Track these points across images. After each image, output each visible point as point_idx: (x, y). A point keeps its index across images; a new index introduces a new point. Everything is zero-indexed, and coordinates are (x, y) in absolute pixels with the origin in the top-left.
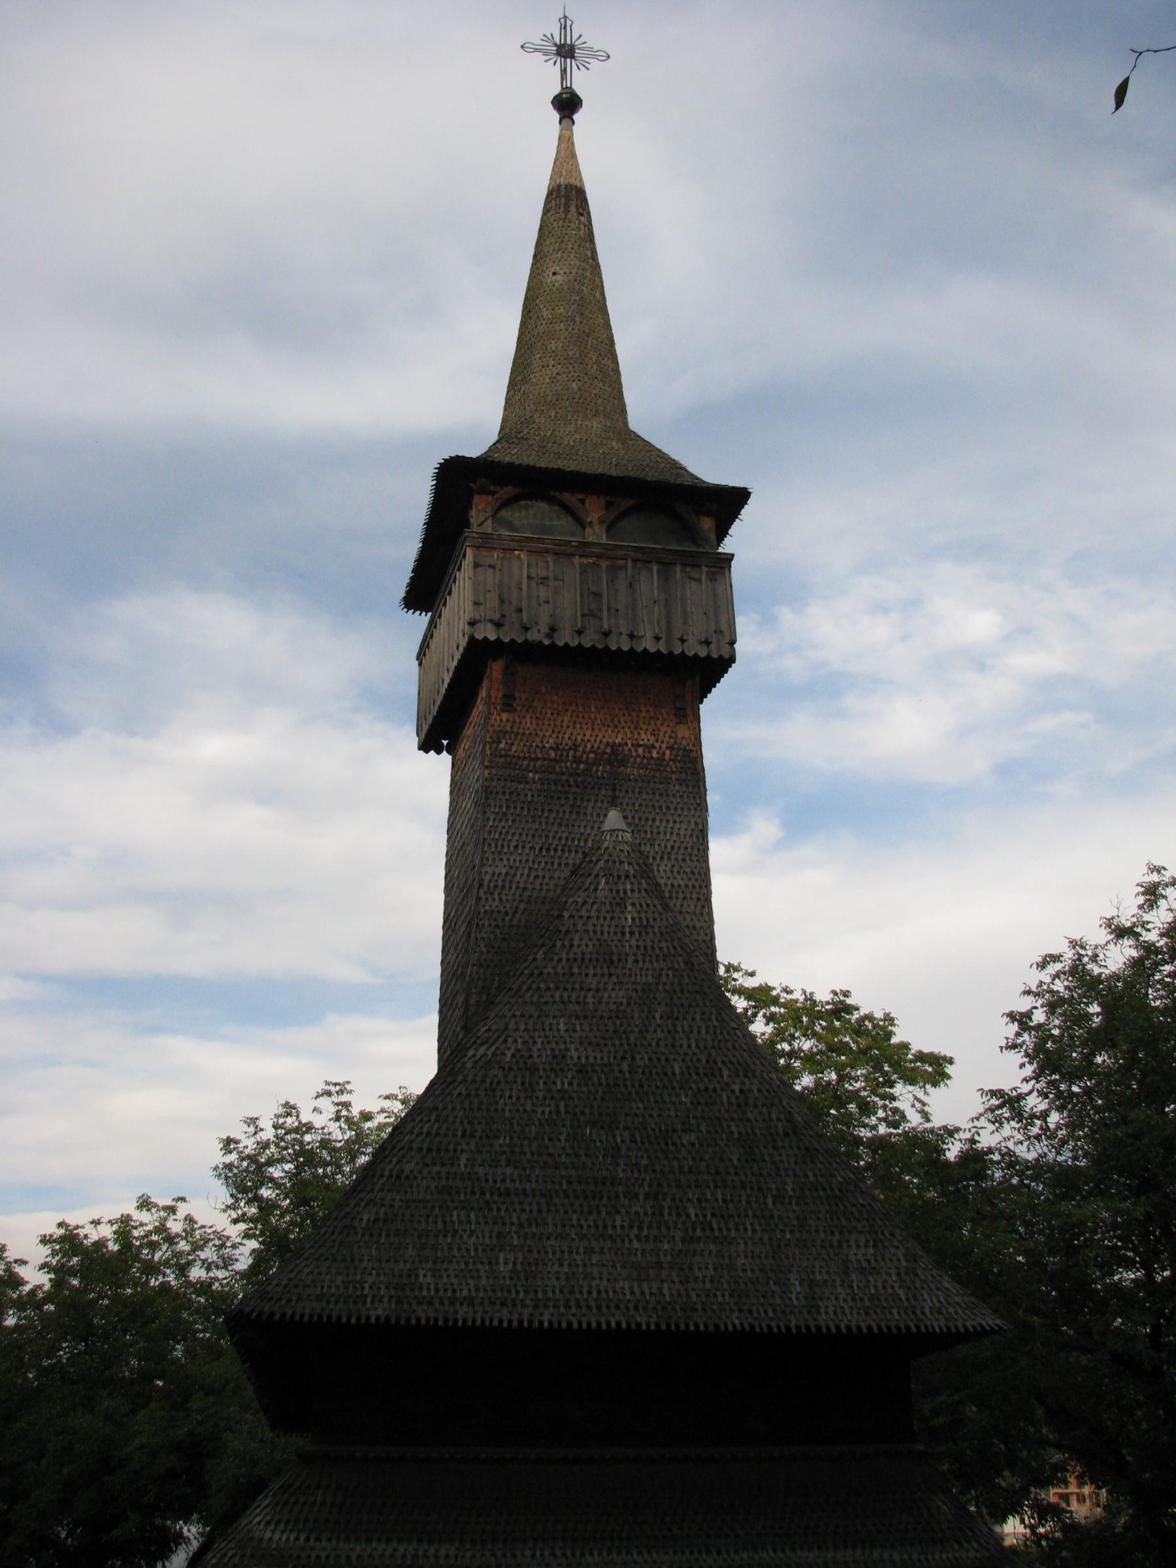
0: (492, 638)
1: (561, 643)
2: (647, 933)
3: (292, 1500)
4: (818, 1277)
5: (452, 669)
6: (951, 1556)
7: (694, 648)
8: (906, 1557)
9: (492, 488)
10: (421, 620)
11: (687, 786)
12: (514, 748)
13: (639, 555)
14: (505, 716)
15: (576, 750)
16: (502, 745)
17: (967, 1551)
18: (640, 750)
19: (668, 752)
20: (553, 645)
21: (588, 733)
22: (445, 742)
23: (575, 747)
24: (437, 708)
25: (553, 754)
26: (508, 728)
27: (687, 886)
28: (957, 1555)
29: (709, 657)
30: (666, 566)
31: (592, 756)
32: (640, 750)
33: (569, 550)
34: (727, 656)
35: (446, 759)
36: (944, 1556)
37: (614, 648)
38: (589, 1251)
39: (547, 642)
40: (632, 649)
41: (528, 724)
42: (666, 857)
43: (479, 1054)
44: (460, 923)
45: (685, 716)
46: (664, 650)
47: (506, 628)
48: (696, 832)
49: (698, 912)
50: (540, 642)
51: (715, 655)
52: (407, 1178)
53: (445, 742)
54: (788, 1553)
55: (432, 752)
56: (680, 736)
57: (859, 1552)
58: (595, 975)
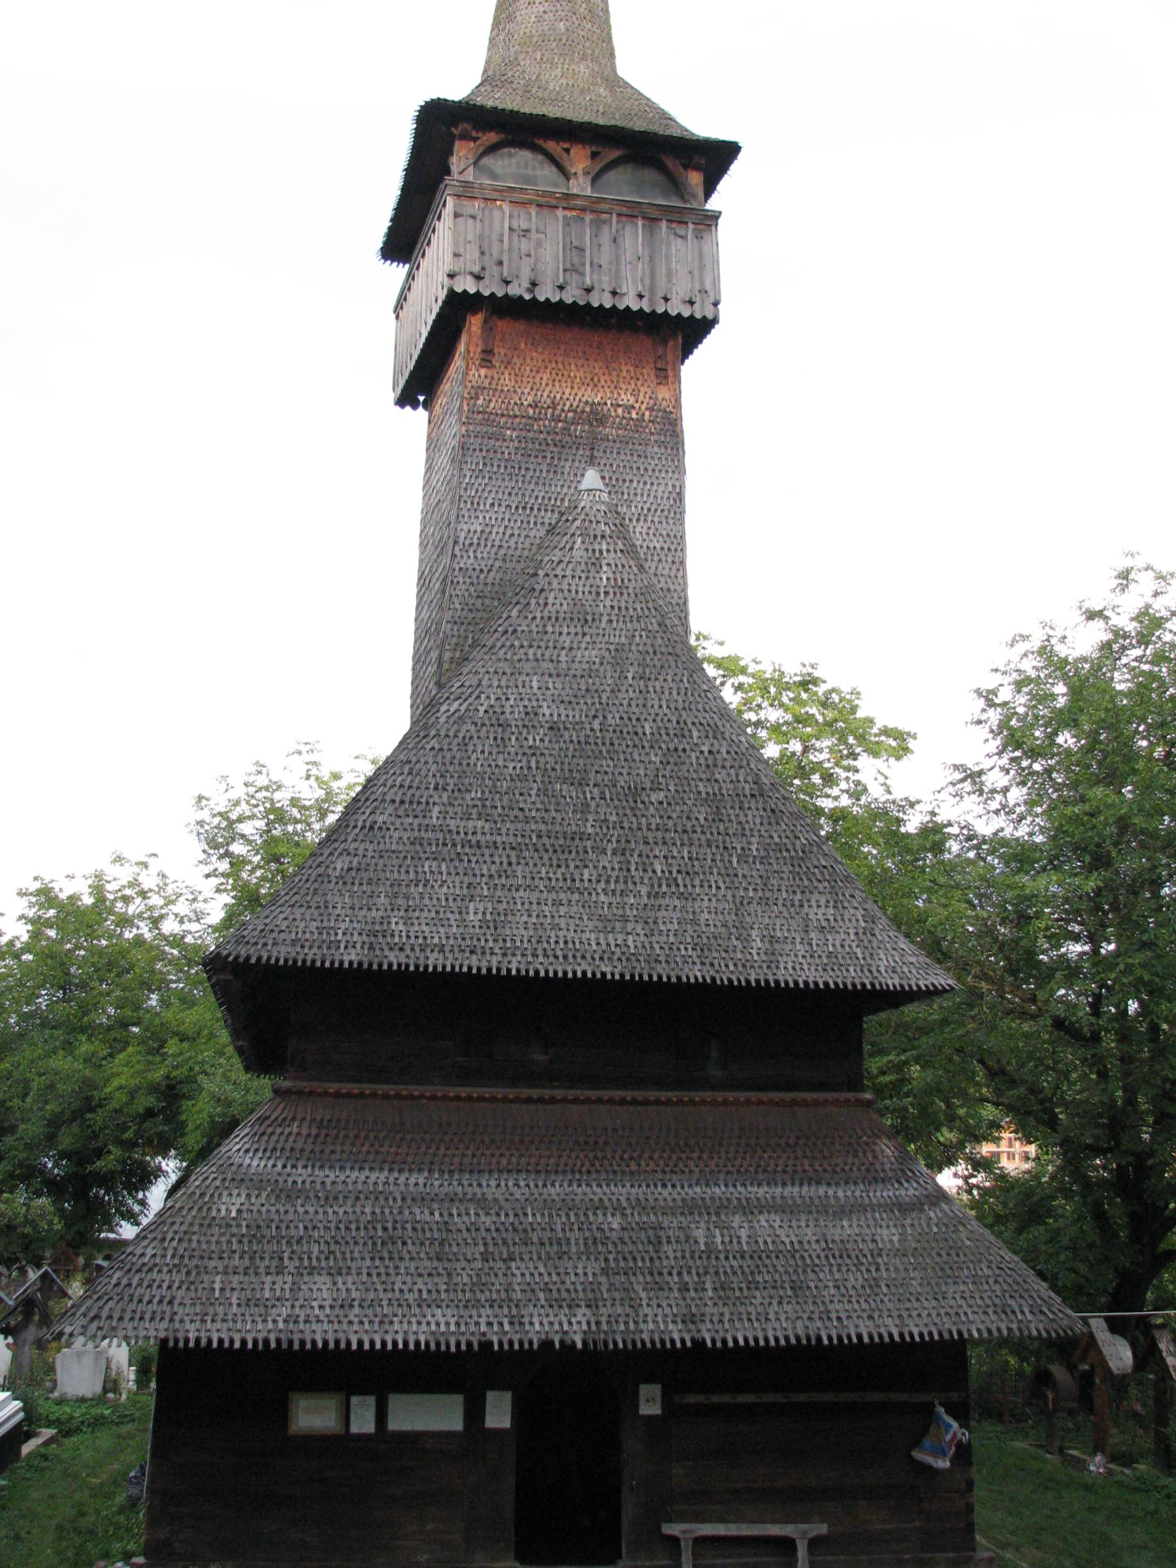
0: (472, 291)
1: (542, 299)
2: (622, 594)
3: (270, 1130)
4: (779, 934)
5: (430, 323)
6: (891, 1194)
7: (676, 308)
8: (849, 1193)
9: (474, 134)
10: (398, 272)
11: (666, 448)
12: (492, 405)
13: (625, 210)
14: (483, 372)
15: (554, 409)
16: (480, 402)
17: (907, 1189)
18: (620, 411)
19: (647, 414)
20: (534, 300)
21: (567, 391)
22: (421, 398)
23: (554, 406)
24: (413, 363)
25: (531, 412)
26: (486, 384)
27: (662, 548)
28: (897, 1193)
29: (692, 317)
30: (652, 221)
31: (570, 415)
32: (620, 411)
33: (553, 202)
34: (710, 317)
35: (422, 414)
36: (885, 1194)
37: (596, 305)
38: (558, 903)
39: (527, 297)
40: (614, 306)
41: (507, 382)
42: (642, 518)
43: (452, 709)
44: (434, 580)
45: (666, 377)
46: (647, 310)
47: (487, 280)
48: (674, 495)
49: (672, 575)
50: (521, 297)
51: (698, 316)
52: (380, 828)
53: (421, 398)
54: (739, 1188)
55: (408, 408)
56: (660, 397)
57: (805, 1188)
58: (569, 634)
